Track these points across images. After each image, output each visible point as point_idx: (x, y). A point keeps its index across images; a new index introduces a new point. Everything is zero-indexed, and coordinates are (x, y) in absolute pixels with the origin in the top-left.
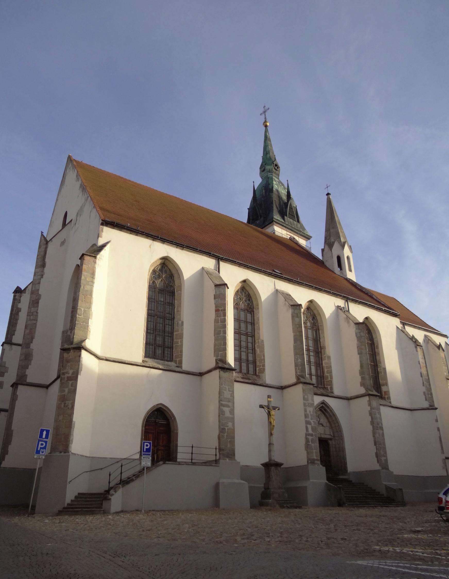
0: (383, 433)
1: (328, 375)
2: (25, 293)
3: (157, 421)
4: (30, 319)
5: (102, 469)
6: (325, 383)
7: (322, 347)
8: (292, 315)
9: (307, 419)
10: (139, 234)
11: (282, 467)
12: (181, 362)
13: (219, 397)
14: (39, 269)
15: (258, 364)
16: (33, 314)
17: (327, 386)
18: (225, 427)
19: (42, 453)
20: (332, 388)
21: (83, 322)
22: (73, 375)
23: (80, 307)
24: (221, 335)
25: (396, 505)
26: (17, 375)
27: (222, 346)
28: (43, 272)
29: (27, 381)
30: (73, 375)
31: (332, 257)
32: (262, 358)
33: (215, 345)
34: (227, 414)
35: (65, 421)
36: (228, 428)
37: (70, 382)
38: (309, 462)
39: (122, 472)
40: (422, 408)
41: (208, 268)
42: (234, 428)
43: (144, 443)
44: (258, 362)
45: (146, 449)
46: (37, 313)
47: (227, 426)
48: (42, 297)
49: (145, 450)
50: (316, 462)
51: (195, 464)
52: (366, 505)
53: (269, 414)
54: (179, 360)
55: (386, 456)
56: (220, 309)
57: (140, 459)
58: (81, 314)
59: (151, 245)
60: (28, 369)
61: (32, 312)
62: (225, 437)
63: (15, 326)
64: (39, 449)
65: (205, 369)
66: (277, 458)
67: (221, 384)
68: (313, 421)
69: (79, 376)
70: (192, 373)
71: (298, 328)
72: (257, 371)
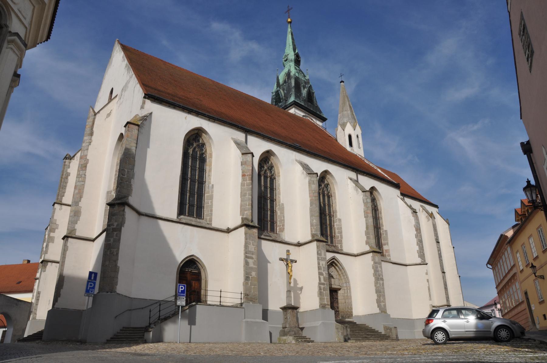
0: (383, 283)
1: (339, 235)
3: (190, 270)
4: (79, 180)
5: (142, 308)
6: (336, 242)
7: (334, 211)
8: (309, 182)
10: (176, 107)
12: (211, 220)
14: (88, 137)
15: (278, 224)
16: (81, 176)
18: (249, 276)
20: (341, 246)
22: (118, 227)
24: (247, 196)
25: (392, 340)
26: (68, 229)
27: (247, 206)
28: (91, 139)
29: (76, 235)
30: (118, 227)
31: (345, 136)
32: (282, 219)
33: (241, 206)
36: (252, 276)
37: (115, 233)
38: (321, 306)
40: (415, 263)
41: (236, 138)
43: (179, 285)
44: (278, 223)
45: (181, 290)
46: (85, 175)
47: (251, 275)
48: (89, 161)
49: (180, 292)
52: (367, 340)
54: (209, 218)
55: (385, 302)
56: (246, 174)
57: (176, 299)
60: (77, 224)
61: (80, 174)
62: (249, 284)
63: (64, 188)
64: (88, 289)
65: (232, 227)
67: (246, 239)
69: (123, 228)
70: (220, 230)
71: (314, 193)
72: (278, 230)
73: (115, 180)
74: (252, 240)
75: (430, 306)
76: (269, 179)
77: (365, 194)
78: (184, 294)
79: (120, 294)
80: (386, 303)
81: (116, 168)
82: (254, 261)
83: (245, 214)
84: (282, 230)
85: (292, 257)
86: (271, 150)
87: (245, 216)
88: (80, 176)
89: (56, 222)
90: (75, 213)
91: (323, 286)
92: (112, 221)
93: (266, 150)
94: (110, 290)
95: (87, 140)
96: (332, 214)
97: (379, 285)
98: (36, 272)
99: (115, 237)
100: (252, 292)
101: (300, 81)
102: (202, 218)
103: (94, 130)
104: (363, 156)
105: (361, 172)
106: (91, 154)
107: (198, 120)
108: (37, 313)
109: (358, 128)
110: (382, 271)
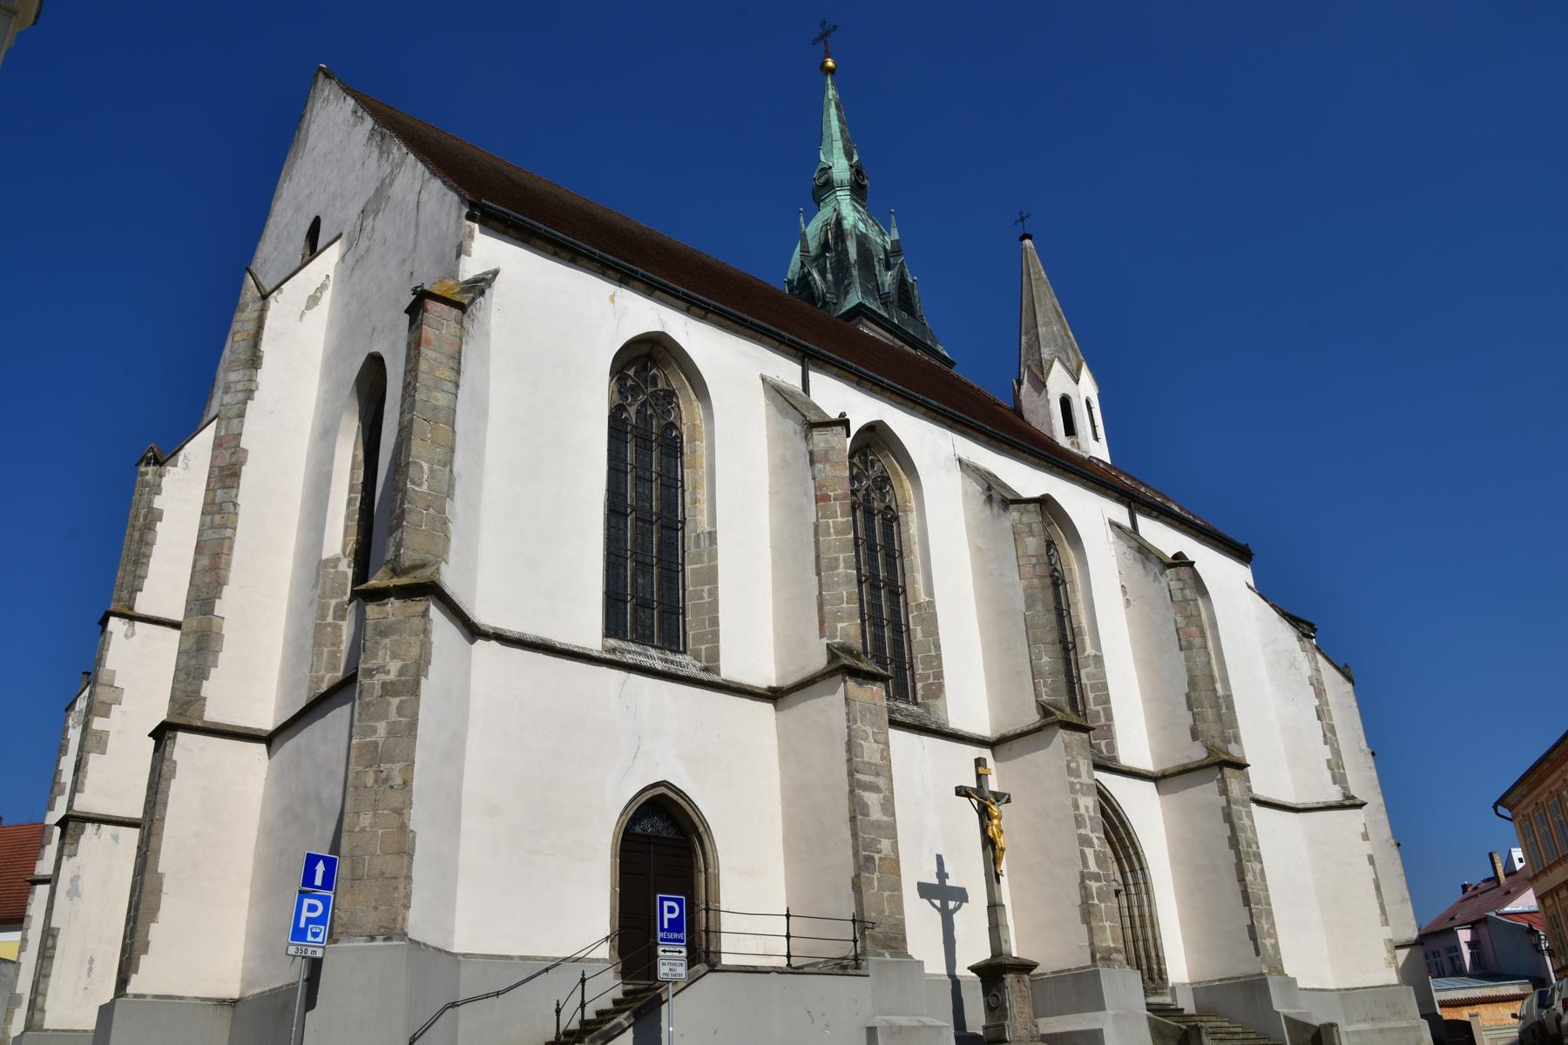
0: (1262, 870)
1: (1099, 708)
2: (175, 465)
4: (212, 522)
5: (498, 994)
7: (1076, 630)
9: (1082, 831)
11: (1035, 972)
12: (714, 655)
13: (849, 760)
15: (920, 671)
17: (1098, 741)
19: (312, 939)
21: (429, 507)
23: (418, 457)
24: (840, 570)
27: (845, 605)
29: (205, 719)
32: (933, 653)
34: (876, 814)
35: (380, 831)
37: (395, 701)
39: (586, 1000)
42: (898, 857)
45: (669, 919)
46: (235, 505)
49: (666, 926)
50: (1114, 956)
51: (801, 971)
53: (984, 813)
55: (1274, 936)
56: (832, 494)
58: (421, 479)
59: (614, 295)
61: (217, 501)
62: (876, 883)
64: (302, 925)
66: (1015, 948)
68: (1098, 835)
71: (1034, 565)
72: (920, 693)
73: (348, 517)
74: (873, 724)
75: (1385, 944)
76: (878, 520)
77: (1178, 574)
78: (679, 933)
79: (419, 943)
80: (1279, 937)
81: (352, 479)
82: (884, 797)
83: (838, 634)
84: (937, 690)
85: (993, 785)
86: (881, 423)
87: (838, 640)
88: (216, 508)
89: (113, 681)
90: (198, 642)
91: (1098, 884)
92: (380, 654)
93: (870, 421)
94: (382, 930)
95: (239, 382)
96: (1069, 640)
97: (1252, 878)
98: (36, 853)
99: (393, 716)
100: (887, 914)
101: (872, 248)
102: (681, 649)
103: (262, 349)
104: (1108, 460)
105: (1143, 505)
106: (255, 432)
107: (652, 309)
108: (46, 1008)
109: (1086, 376)
110: (1255, 829)
